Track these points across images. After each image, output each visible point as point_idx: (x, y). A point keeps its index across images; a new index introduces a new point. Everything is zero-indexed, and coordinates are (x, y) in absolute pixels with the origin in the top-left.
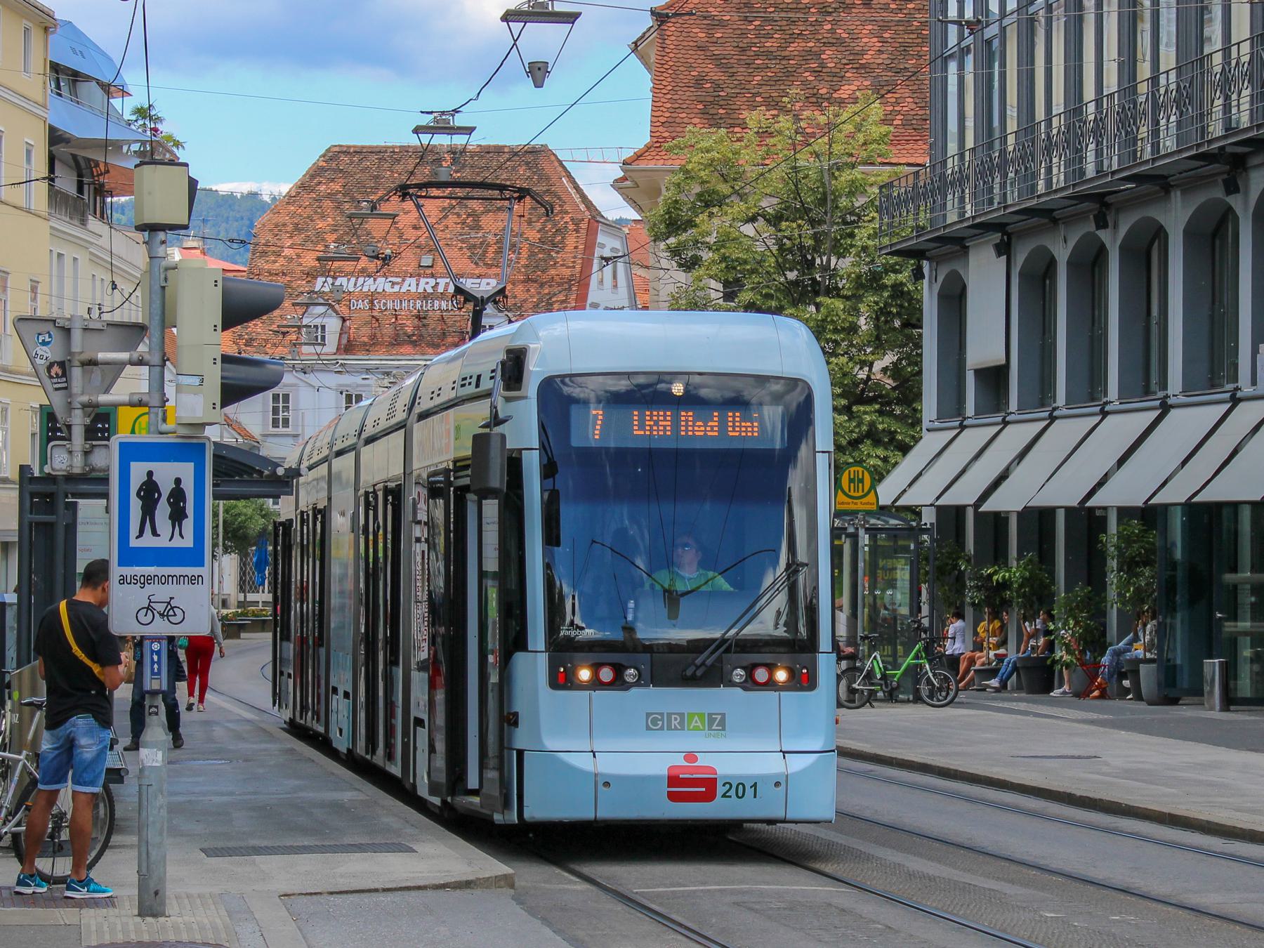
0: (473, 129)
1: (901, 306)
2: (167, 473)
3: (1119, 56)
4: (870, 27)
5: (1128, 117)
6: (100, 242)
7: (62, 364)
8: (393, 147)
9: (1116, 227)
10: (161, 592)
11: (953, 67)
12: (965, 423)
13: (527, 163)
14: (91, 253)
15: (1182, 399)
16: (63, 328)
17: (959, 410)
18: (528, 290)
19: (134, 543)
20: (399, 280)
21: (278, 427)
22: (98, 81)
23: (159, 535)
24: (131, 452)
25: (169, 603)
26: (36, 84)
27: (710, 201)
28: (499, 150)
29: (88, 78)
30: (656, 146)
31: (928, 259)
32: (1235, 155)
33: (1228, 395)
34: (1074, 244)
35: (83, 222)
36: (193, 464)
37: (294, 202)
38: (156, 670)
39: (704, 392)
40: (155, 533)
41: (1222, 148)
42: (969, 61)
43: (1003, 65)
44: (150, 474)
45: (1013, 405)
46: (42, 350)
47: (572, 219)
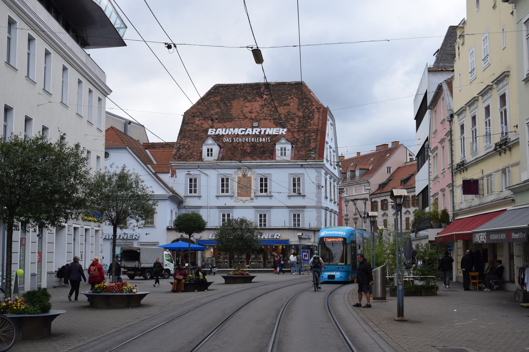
8: (241, 84)
13: (296, 88)
18: (299, 135)
20: (245, 129)
21: (263, 192)
37: (200, 104)
39: (431, 177)
47: (316, 108)
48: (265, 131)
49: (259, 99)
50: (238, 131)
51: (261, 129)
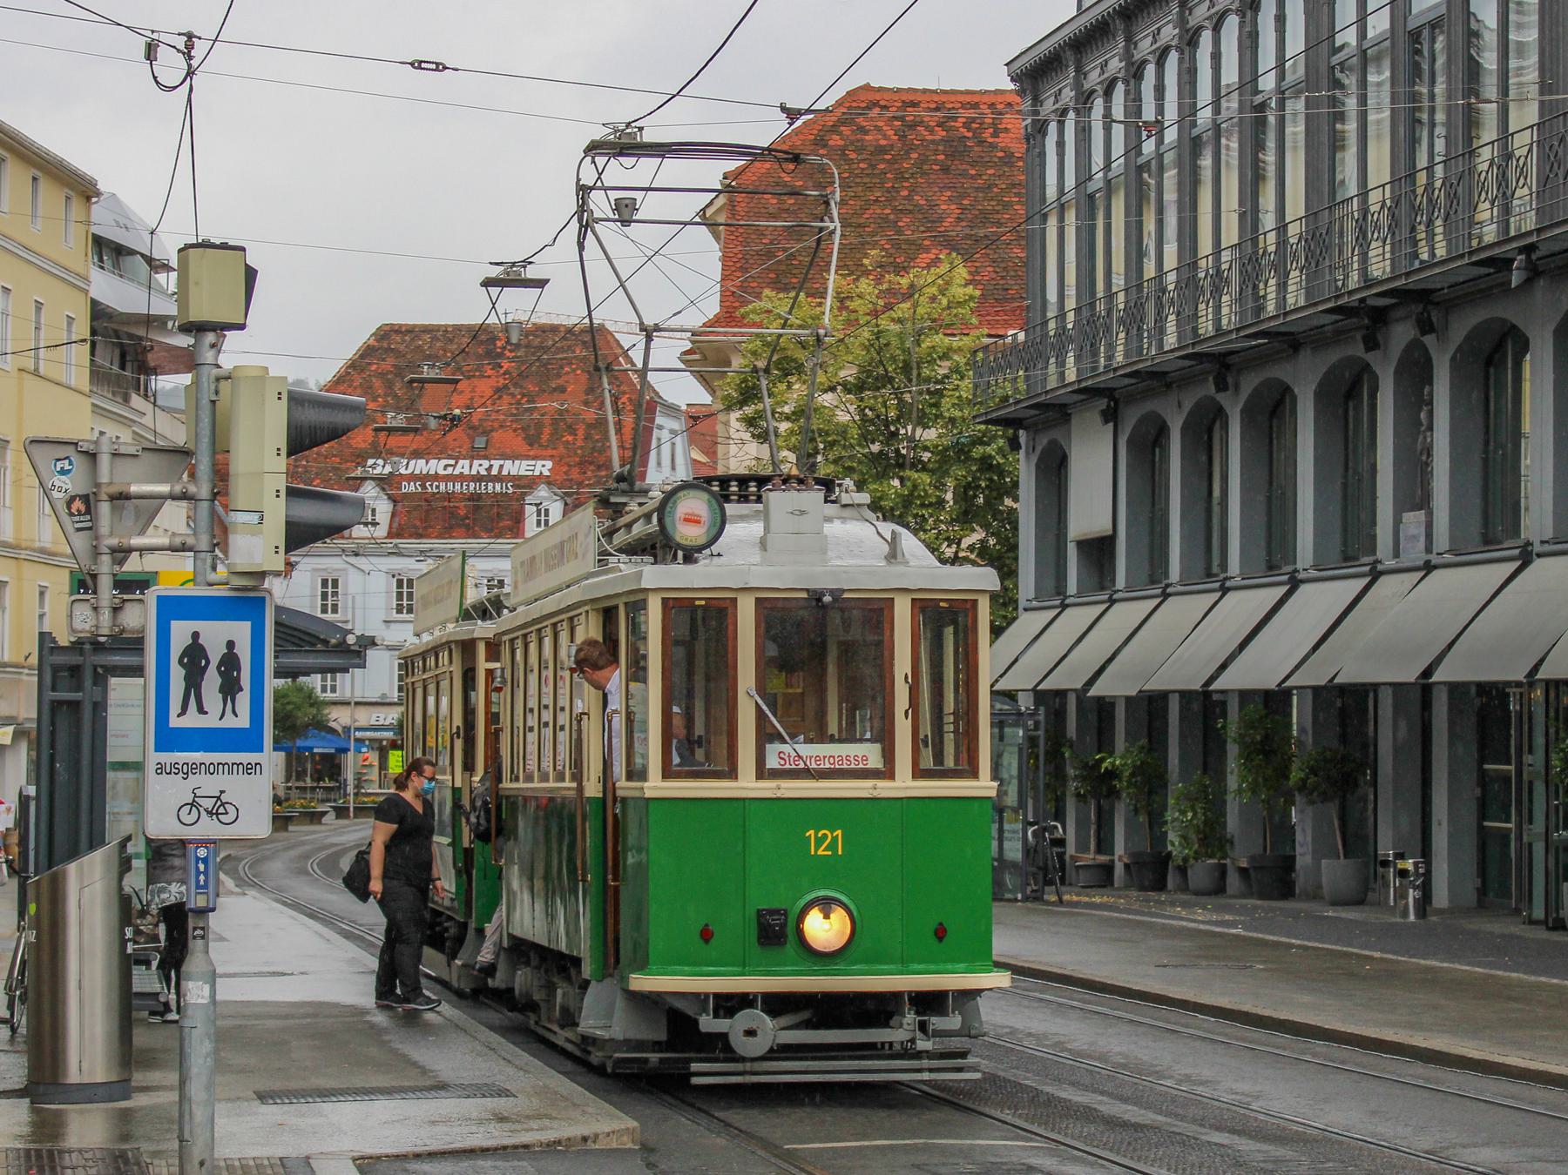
0: (545, 282)
1: (991, 480)
2: (216, 634)
3: (1240, 205)
4: (949, 194)
5: (1251, 262)
6: (143, 421)
7: (85, 499)
8: (446, 326)
9: (1237, 387)
10: (209, 785)
11: (1052, 222)
12: (1115, 597)
14: (134, 432)
15: (1313, 573)
16: (86, 453)
17: (1060, 590)
19: (175, 722)
20: (452, 462)
22: (143, 255)
23: (206, 713)
24: (172, 608)
25: (219, 798)
26: (75, 252)
27: (788, 368)
28: (554, 329)
29: (132, 252)
30: (728, 316)
31: (1025, 429)
32: (1375, 309)
33: (1368, 568)
34: (1249, 391)
35: (126, 399)
36: (249, 624)
38: (202, 883)
40: (201, 710)
41: (1362, 300)
42: (1071, 217)
43: (1108, 215)
44: (196, 635)
45: (1121, 581)
46: (59, 480)
48: (501, 466)
49: (490, 372)
50: (436, 466)
51: (492, 462)
